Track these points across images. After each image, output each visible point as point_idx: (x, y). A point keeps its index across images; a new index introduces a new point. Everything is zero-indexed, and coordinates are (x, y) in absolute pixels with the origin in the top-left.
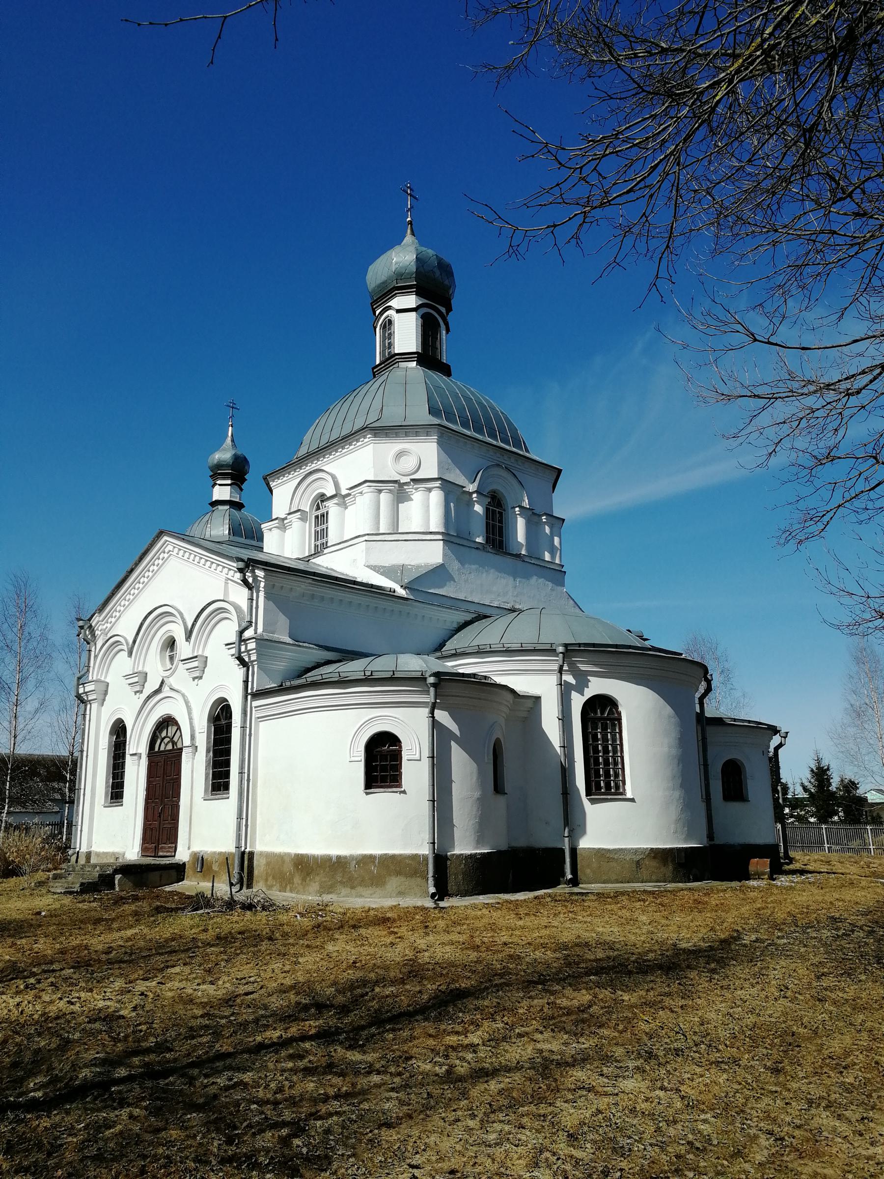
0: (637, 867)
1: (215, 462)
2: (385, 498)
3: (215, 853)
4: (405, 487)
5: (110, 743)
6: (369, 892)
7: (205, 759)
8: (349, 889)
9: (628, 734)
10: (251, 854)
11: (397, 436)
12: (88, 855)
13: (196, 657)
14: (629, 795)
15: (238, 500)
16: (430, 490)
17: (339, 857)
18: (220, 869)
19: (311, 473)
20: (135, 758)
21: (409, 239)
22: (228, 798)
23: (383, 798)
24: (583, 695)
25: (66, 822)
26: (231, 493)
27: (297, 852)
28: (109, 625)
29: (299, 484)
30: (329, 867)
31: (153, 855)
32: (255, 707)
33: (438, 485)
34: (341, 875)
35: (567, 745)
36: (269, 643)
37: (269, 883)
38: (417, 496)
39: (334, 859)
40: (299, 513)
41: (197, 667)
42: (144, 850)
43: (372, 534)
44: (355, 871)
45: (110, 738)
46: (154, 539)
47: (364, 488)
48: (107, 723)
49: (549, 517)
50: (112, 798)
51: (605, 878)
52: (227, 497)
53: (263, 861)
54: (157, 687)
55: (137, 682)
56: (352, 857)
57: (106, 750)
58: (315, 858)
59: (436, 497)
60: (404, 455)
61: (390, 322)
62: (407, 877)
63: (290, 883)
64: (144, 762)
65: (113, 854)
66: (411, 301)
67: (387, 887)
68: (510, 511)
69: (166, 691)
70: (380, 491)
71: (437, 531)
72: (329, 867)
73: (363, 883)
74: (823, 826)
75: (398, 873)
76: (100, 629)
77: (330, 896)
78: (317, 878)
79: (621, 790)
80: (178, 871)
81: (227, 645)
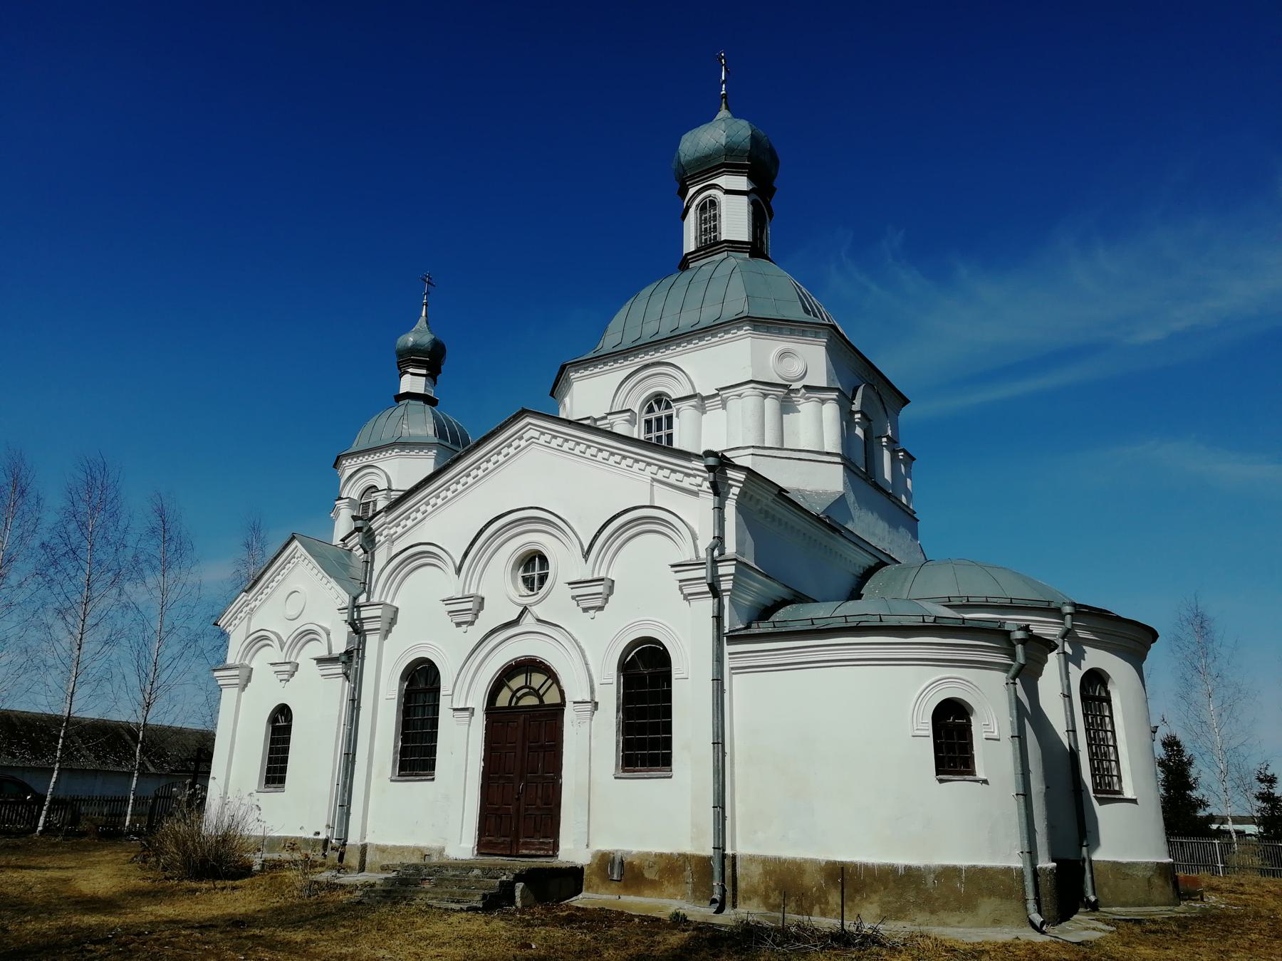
0: (1149, 886)
2: (771, 405)
3: (648, 854)
5: (400, 691)
7: (615, 720)
8: (928, 914)
9: (1125, 717)
10: (734, 857)
11: (780, 332)
12: (364, 849)
15: (432, 395)
16: (823, 401)
17: (908, 869)
18: (661, 877)
19: (646, 366)
20: (467, 714)
21: (723, 113)
22: (671, 777)
23: (958, 787)
24: (1080, 668)
25: (132, 797)
26: (426, 386)
28: (400, 530)
31: (508, 852)
32: (730, 654)
33: (835, 397)
36: (744, 568)
37: (771, 901)
38: (807, 408)
39: (901, 871)
40: (629, 414)
41: (601, 594)
42: (485, 843)
43: (758, 447)
44: (934, 889)
45: (400, 684)
46: (509, 419)
47: (746, 390)
48: (396, 663)
49: (906, 456)
51: (1123, 899)
53: (757, 871)
55: (470, 610)
56: (928, 869)
57: (396, 701)
58: (868, 869)
59: (831, 411)
60: (790, 357)
61: (713, 203)
62: (1002, 898)
63: (819, 902)
66: (741, 183)
68: (876, 441)
69: (528, 623)
70: (765, 396)
71: (834, 451)
73: (945, 906)
74: (1216, 842)
77: (900, 924)
78: (875, 898)
79: (1117, 788)
80: (573, 878)
81: (673, 566)
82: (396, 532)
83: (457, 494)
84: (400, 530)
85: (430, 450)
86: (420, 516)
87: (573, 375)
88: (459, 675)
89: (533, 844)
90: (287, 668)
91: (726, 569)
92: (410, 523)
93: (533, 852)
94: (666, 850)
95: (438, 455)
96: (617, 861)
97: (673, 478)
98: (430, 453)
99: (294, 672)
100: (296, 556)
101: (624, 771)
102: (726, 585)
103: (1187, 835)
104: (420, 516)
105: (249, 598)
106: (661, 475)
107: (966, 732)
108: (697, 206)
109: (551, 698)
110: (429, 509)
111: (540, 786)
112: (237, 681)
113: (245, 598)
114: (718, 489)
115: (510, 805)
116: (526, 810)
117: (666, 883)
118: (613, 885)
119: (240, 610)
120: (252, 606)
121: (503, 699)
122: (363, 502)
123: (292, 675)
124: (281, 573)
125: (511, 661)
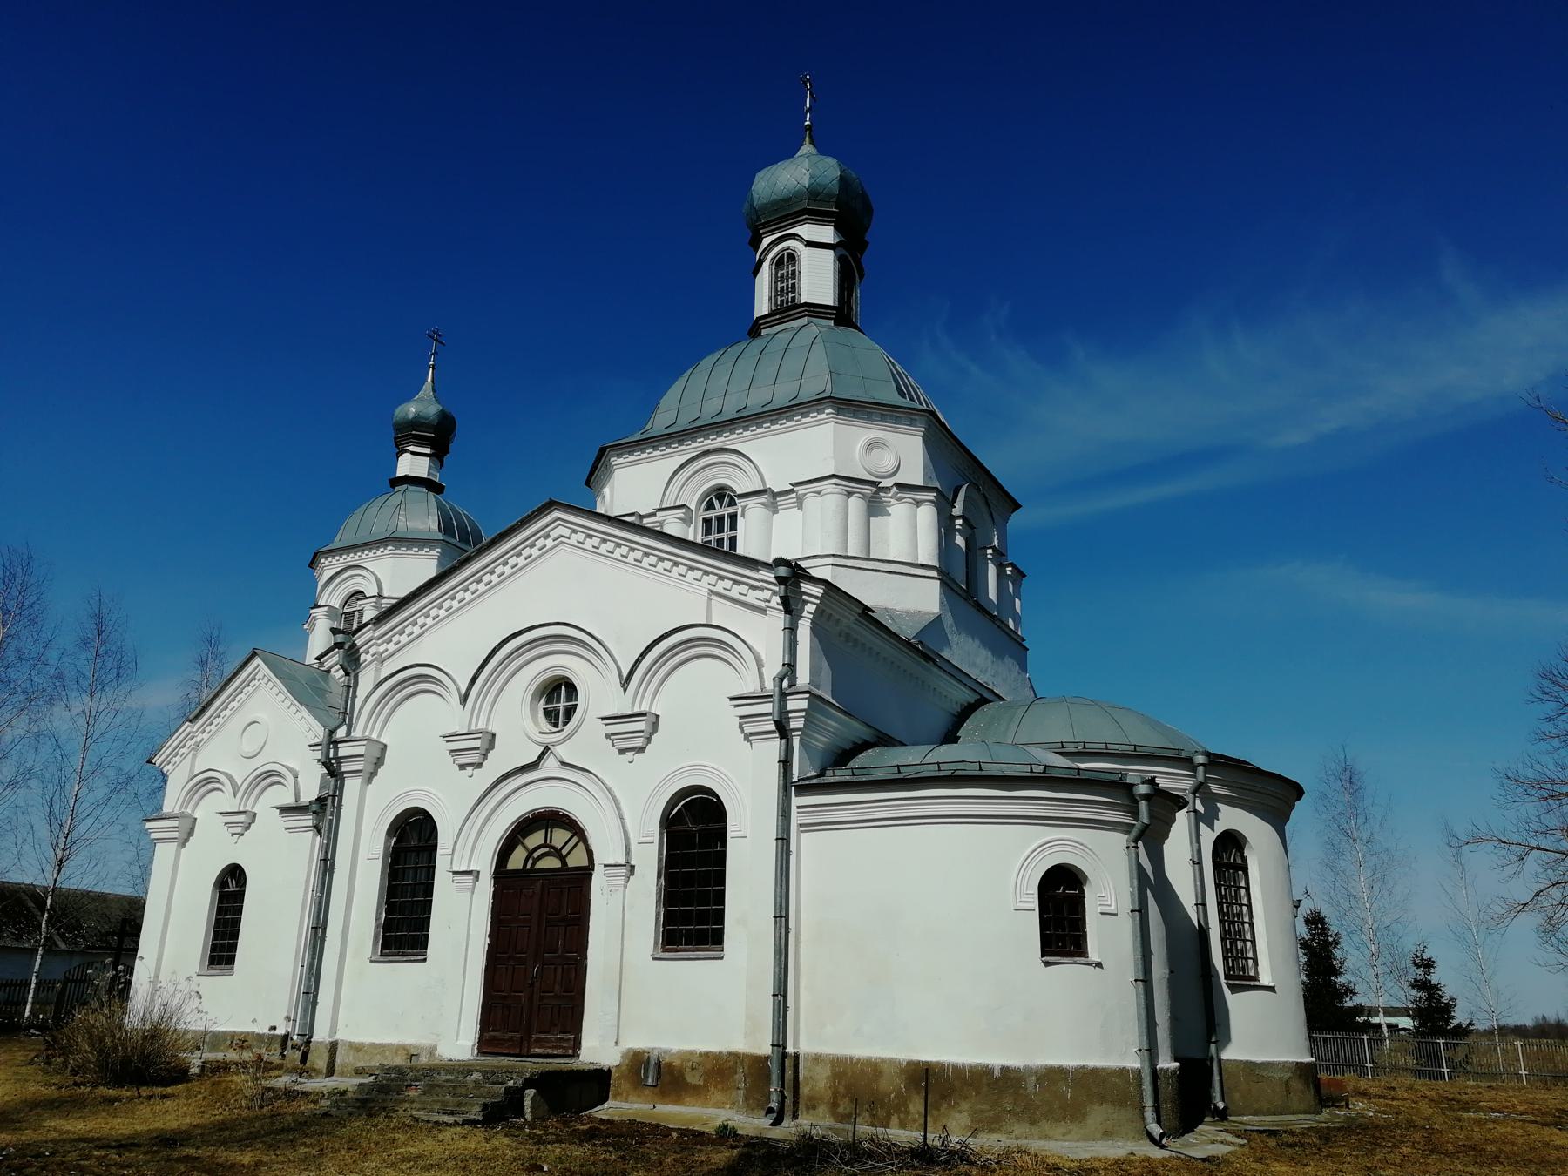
1: (411, 416)
2: (856, 505)
3: (692, 1053)
4: (881, 494)
5: (386, 848)
6: (1061, 1130)
10: (796, 1056)
11: (869, 417)
12: (333, 1047)
13: (645, 714)
14: (1265, 980)
16: (918, 503)
17: (1005, 1070)
18: (706, 1081)
20: (470, 878)
21: (807, 148)
23: (1067, 972)
26: (429, 469)
27: (820, 1052)
28: (391, 647)
29: (682, 467)
30: (988, 1085)
31: (517, 1051)
32: (798, 807)
33: (932, 498)
34: (1011, 1100)
35: (1202, 905)
37: (841, 1110)
38: (898, 510)
39: (997, 1073)
40: (683, 510)
41: (642, 732)
42: (488, 1041)
44: (1035, 1094)
45: (387, 841)
47: (827, 486)
50: (383, 947)
52: (423, 473)
54: (534, 759)
57: (379, 863)
58: (958, 1070)
60: (879, 448)
61: (792, 257)
64: (485, 888)
65: (404, 1048)
66: (827, 233)
67: (1089, 1122)
69: (550, 767)
70: (850, 494)
71: (930, 564)
72: (988, 1085)
75: (1102, 1099)
76: (372, 651)
78: (965, 1105)
79: (1252, 973)
80: (598, 1082)
81: (732, 699)
82: (387, 650)
83: (464, 604)
84: (391, 647)
85: (432, 548)
86: (417, 630)
87: (615, 461)
88: (461, 829)
89: (548, 1040)
90: (241, 818)
91: (797, 704)
92: (404, 639)
93: (549, 1051)
94: (714, 1048)
95: (442, 554)
96: (653, 1062)
97: (736, 591)
98: (432, 552)
99: (250, 824)
100: (257, 677)
101: (665, 951)
102: (796, 723)
103: (1331, 1029)
104: (417, 630)
105: (195, 730)
106: (721, 586)
107: (1078, 905)
108: (773, 259)
109: (577, 859)
110: (429, 621)
111: (559, 970)
112: (175, 835)
113: (189, 729)
114: (791, 606)
115: (521, 992)
116: (542, 998)
117: (713, 1089)
118: (647, 1091)
119: (182, 745)
120: (198, 739)
121: (516, 861)
122: (345, 611)
123: (248, 828)
124: (237, 699)
125: (528, 813)
